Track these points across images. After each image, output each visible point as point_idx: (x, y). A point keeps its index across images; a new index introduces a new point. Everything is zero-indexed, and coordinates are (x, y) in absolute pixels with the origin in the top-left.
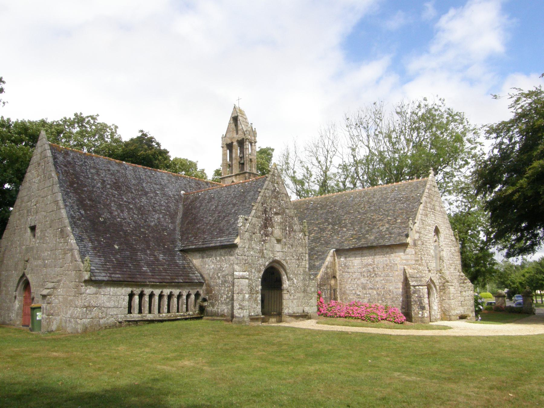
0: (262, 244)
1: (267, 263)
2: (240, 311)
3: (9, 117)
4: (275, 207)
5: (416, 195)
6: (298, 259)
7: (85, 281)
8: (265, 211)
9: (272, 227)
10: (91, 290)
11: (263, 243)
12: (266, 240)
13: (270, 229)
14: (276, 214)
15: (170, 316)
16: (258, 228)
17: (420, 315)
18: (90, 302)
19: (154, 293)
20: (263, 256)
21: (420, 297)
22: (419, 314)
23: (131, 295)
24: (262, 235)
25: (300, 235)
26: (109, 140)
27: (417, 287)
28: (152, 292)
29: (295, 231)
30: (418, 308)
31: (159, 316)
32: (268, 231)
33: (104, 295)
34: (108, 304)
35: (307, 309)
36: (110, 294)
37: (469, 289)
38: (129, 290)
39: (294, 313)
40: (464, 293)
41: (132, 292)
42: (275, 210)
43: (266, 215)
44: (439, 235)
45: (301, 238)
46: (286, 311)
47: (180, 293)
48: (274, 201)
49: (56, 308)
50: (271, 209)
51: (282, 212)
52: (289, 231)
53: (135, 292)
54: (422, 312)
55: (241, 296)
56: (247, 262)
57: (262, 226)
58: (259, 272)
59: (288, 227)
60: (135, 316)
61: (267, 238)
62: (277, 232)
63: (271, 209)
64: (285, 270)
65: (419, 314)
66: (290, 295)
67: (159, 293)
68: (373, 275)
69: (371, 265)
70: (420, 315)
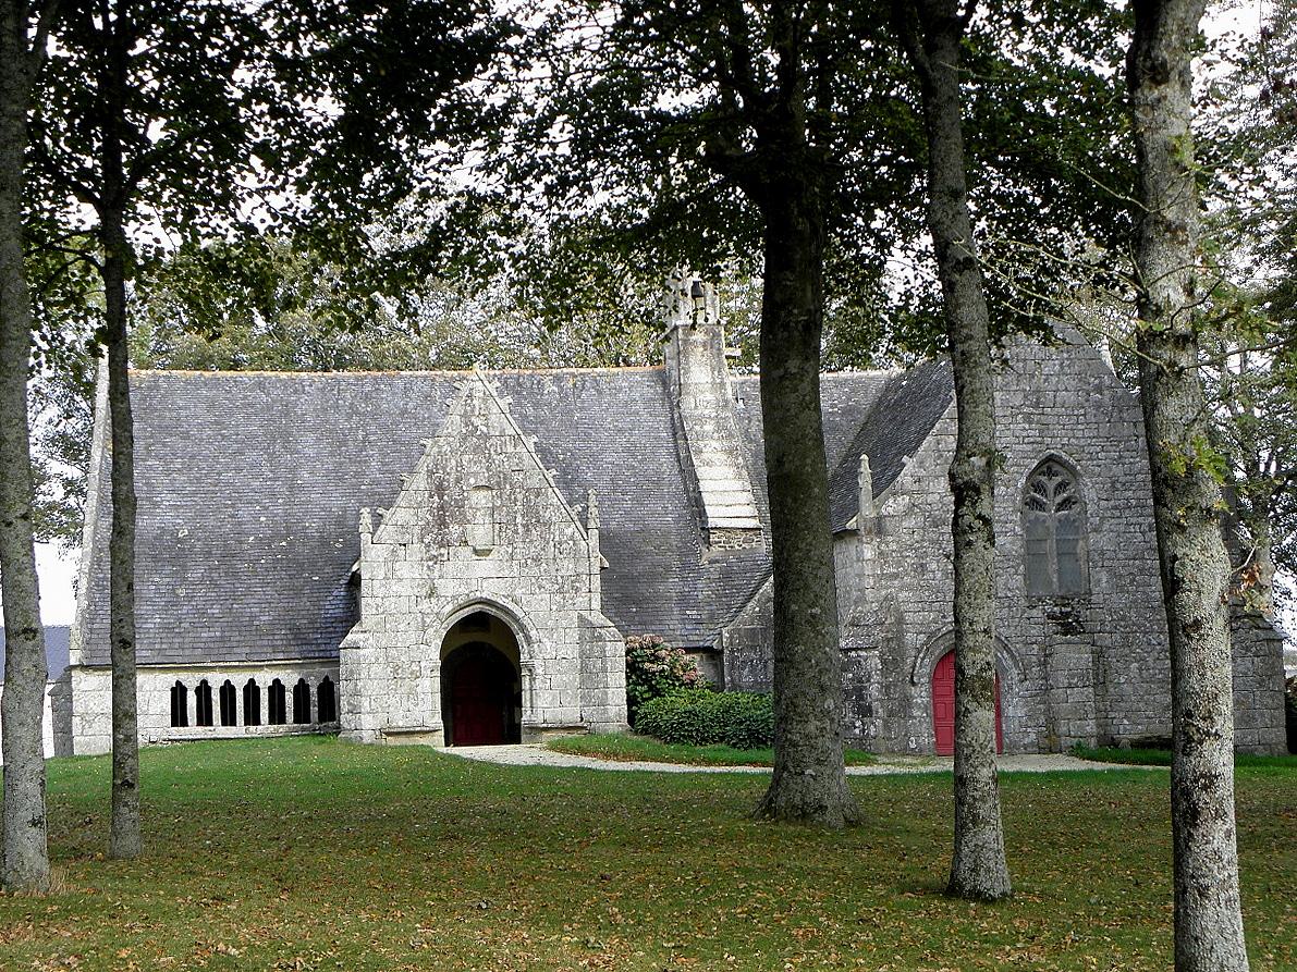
0: (428, 567)
2: (349, 716)
4: (475, 474)
6: (560, 591)
8: (440, 489)
9: (464, 521)
11: (431, 563)
12: (442, 555)
14: (478, 488)
16: (417, 530)
17: (857, 731)
21: (860, 681)
22: (855, 727)
23: (179, 693)
24: (428, 545)
27: (853, 654)
29: (548, 524)
30: (854, 713)
37: (1248, 649)
38: (171, 679)
41: (178, 683)
42: (472, 481)
43: (441, 498)
45: (572, 538)
47: (301, 680)
51: (498, 483)
54: (863, 724)
55: (351, 686)
56: (381, 610)
61: (443, 551)
62: (480, 533)
63: (458, 481)
64: (523, 628)
65: (855, 727)
70: (857, 731)
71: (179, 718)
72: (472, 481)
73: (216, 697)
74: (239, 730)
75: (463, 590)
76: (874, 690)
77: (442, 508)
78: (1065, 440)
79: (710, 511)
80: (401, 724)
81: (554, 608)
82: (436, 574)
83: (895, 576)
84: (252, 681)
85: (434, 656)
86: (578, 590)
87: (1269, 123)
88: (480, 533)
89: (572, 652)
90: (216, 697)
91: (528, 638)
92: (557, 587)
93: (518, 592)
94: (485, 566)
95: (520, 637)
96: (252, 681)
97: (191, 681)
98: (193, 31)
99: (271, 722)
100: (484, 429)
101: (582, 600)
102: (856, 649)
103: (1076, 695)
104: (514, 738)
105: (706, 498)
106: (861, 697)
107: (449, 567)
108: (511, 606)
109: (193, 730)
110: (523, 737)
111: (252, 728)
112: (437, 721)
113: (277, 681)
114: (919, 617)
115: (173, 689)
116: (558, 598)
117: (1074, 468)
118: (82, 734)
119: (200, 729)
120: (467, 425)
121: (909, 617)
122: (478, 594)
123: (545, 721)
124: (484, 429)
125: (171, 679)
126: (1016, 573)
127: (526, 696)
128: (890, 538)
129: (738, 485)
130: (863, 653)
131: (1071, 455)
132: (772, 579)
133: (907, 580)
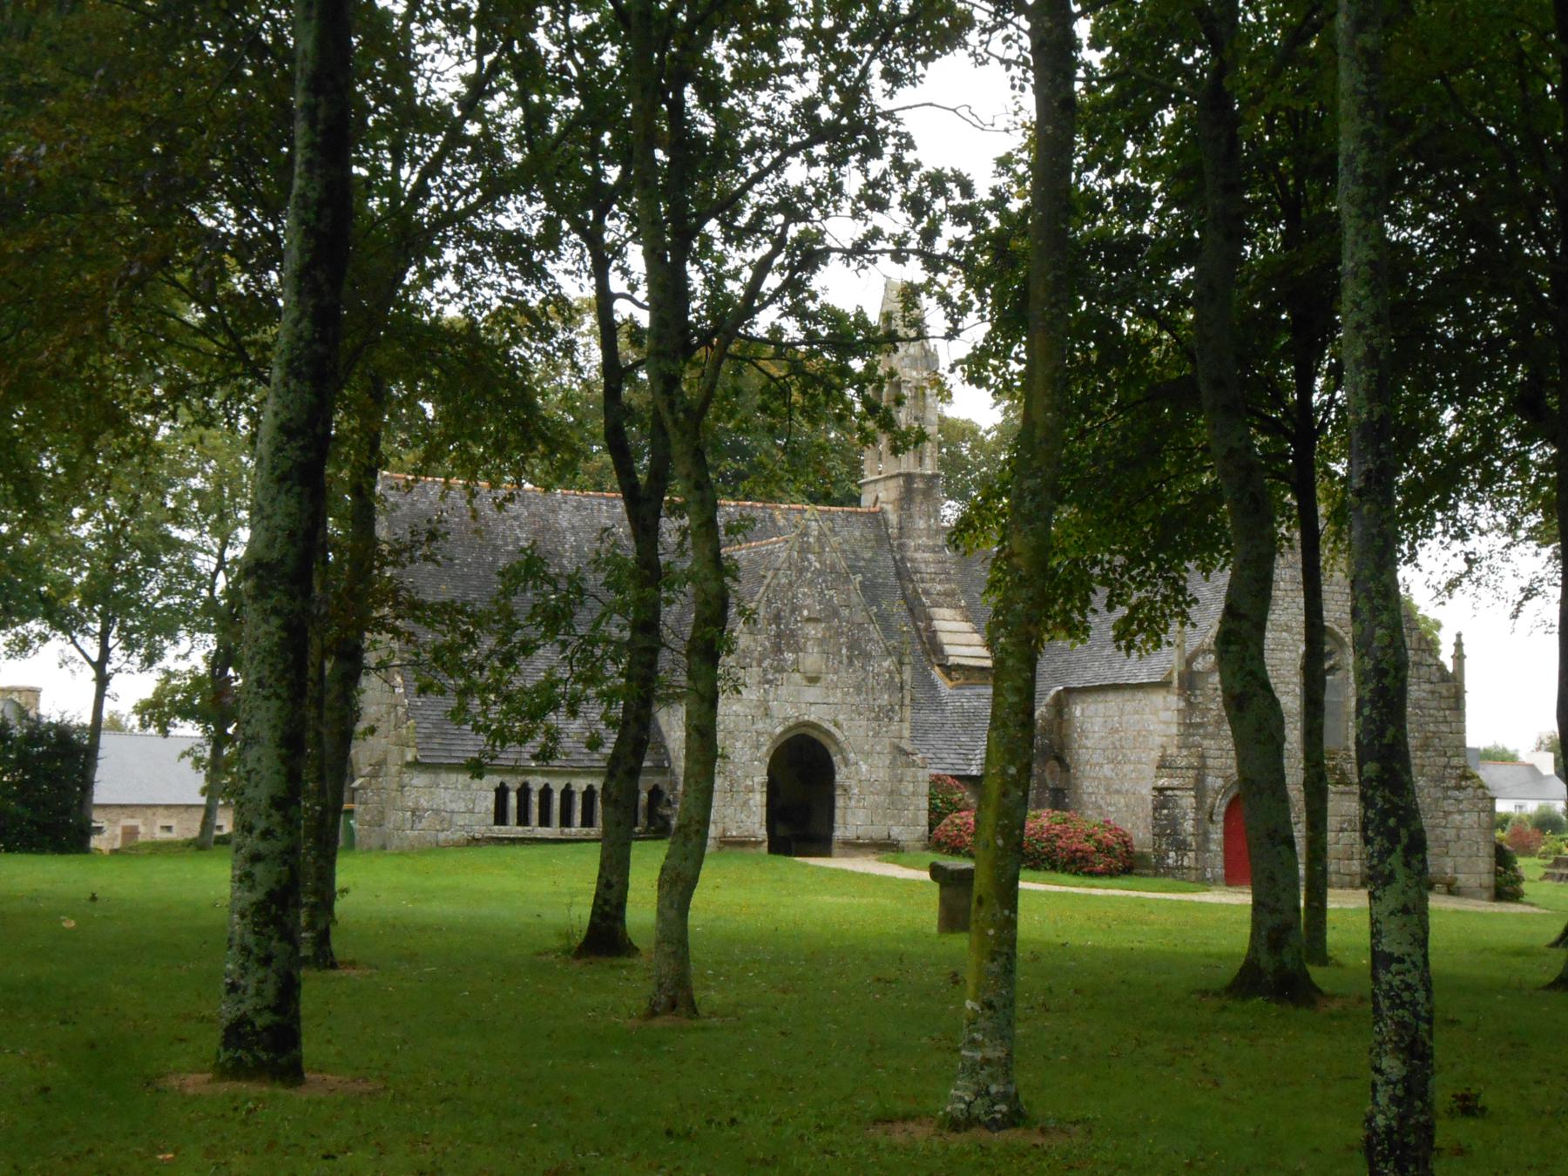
1: (779, 730)
3: (1443, 623)
5: (1071, 426)
6: (877, 719)
7: (408, 765)
9: (798, 649)
10: (420, 780)
11: (767, 686)
12: (776, 679)
13: (789, 656)
14: (809, 620)
15: (588, 834)
18: (418, 802)
19: (551, 786)
20: (767, 714)
23: (501, 792)
24: (765, 670)
25: (886, 664)
26: (810, 556)
28: (547, 785)
29: (867, 656)
31: (562, 833)
32: (785, 660)
33: (446, 788)
34: (454, 806)
35: (896, 832)
36: (456, 788)
39: (858, 838)
40: (1457, 817)
41: (502, 784)
42: (805, 613)
43: (778, 627)
44: (1493, 852)
46: (839, 833)
48: (804, 594)
49: (1371, 584)
50: (793, 611)
52: (848, 657)
53: (508, 785)
57: (765, 649)
58: (758, 747)
59: (848, 648)
60: (512, 829)
61: (777, 675)
62: (812, 659)
63: (793, 611)
64: (841, 751)
66: (850, 799)
67: (563, 787)
68: (1120, 758)
69: (1117, 731)
71: (500, 817)
72: (805, 613)
73: (556, 797)
74: (553, 831)
75: (791, 711)
76: (1188, 826)
77: (778, 635)
78: (1338, 615)
79: (948, 649)
80: (734, 834)
81: (871, 734)
82: (771, 696)
83: (1201, 725)
84: (568, 786)
85: (760, 777)
86: (891, 719)
87: (864, 9)
88: (812, 659)
89: (883, 774)
90: (556, 797)
91: (846, 762)
92: (873, 715)
93: (841, 718)
94: (813, 693)
95: (836, 759)
96: (568, 786)
97: (513, 783)
98: (689, 201)
99: (583, 825)
100: (818, 565)
101: (894, 727)
102: (1172, 789)
103: (1345, 837)
104: (826, 852)
105: (944, 638)
106: (1175, 833)
107: (782, 691)
108: (833, 729)
109: (512, 829)
110: (836, 850)
111: (567, 830)
112: (762, 833)
113: (590, 787)
114: (1217, 763)
115: (497, 790)
116: (874, 724)
117: (1342, 638)
118: (412, 828)
119: (520, 828)
120: (813, 396)
121: (1210, 762)
122: (806, 718)
123: (858, 838)
124: (818, 565)
125: (495, 780)
126: (1295, 729)
127: (838, 813)
128: (1198, 692)
129: (966, 626)
130: (1178, 793)
131: (1341, 627)
132: (1450, 668)
133: (1210, 729)
